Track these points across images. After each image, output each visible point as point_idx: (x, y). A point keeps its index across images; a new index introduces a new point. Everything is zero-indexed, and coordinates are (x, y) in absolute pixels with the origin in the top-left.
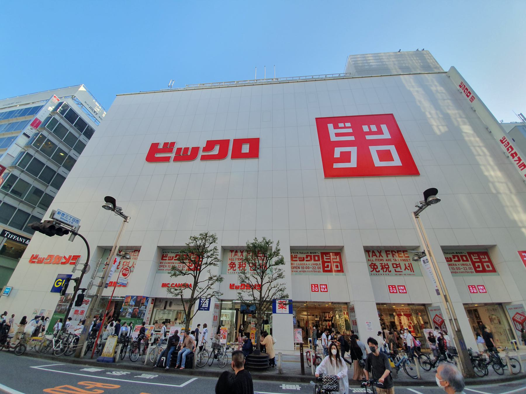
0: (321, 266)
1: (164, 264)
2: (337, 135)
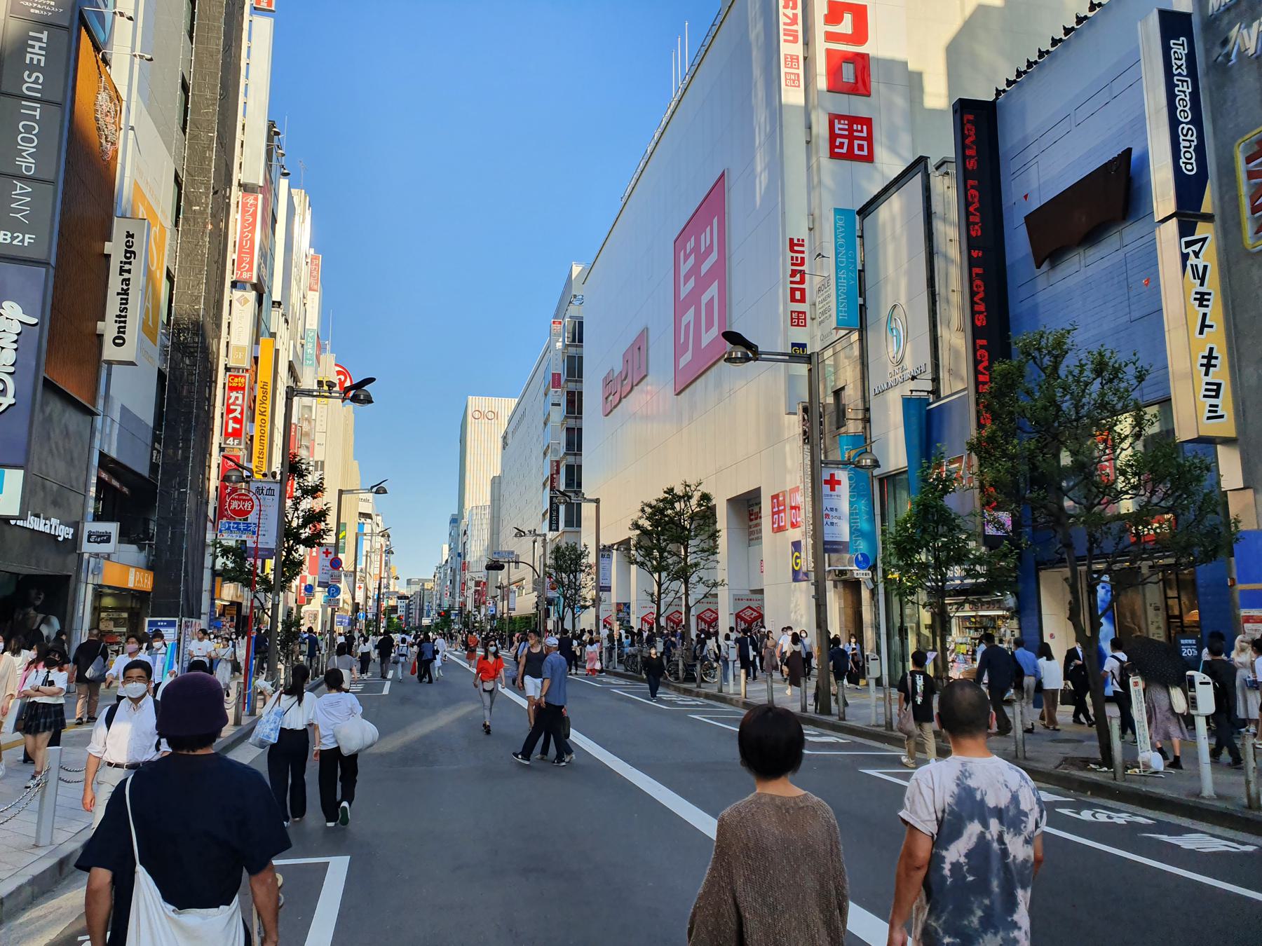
2: (840, 129)
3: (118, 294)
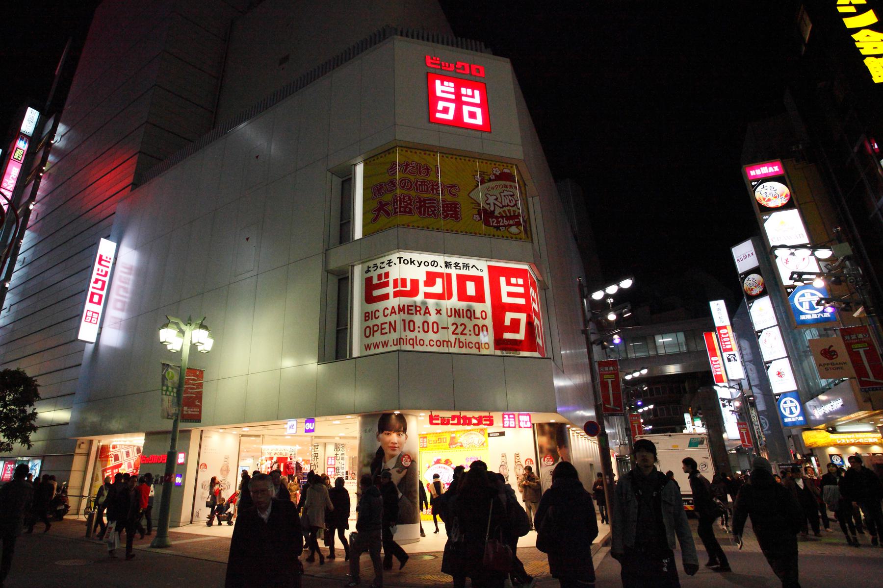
0: (489, 322)
1: (382, 319)
2: (510, 294)
3: (411, 259)
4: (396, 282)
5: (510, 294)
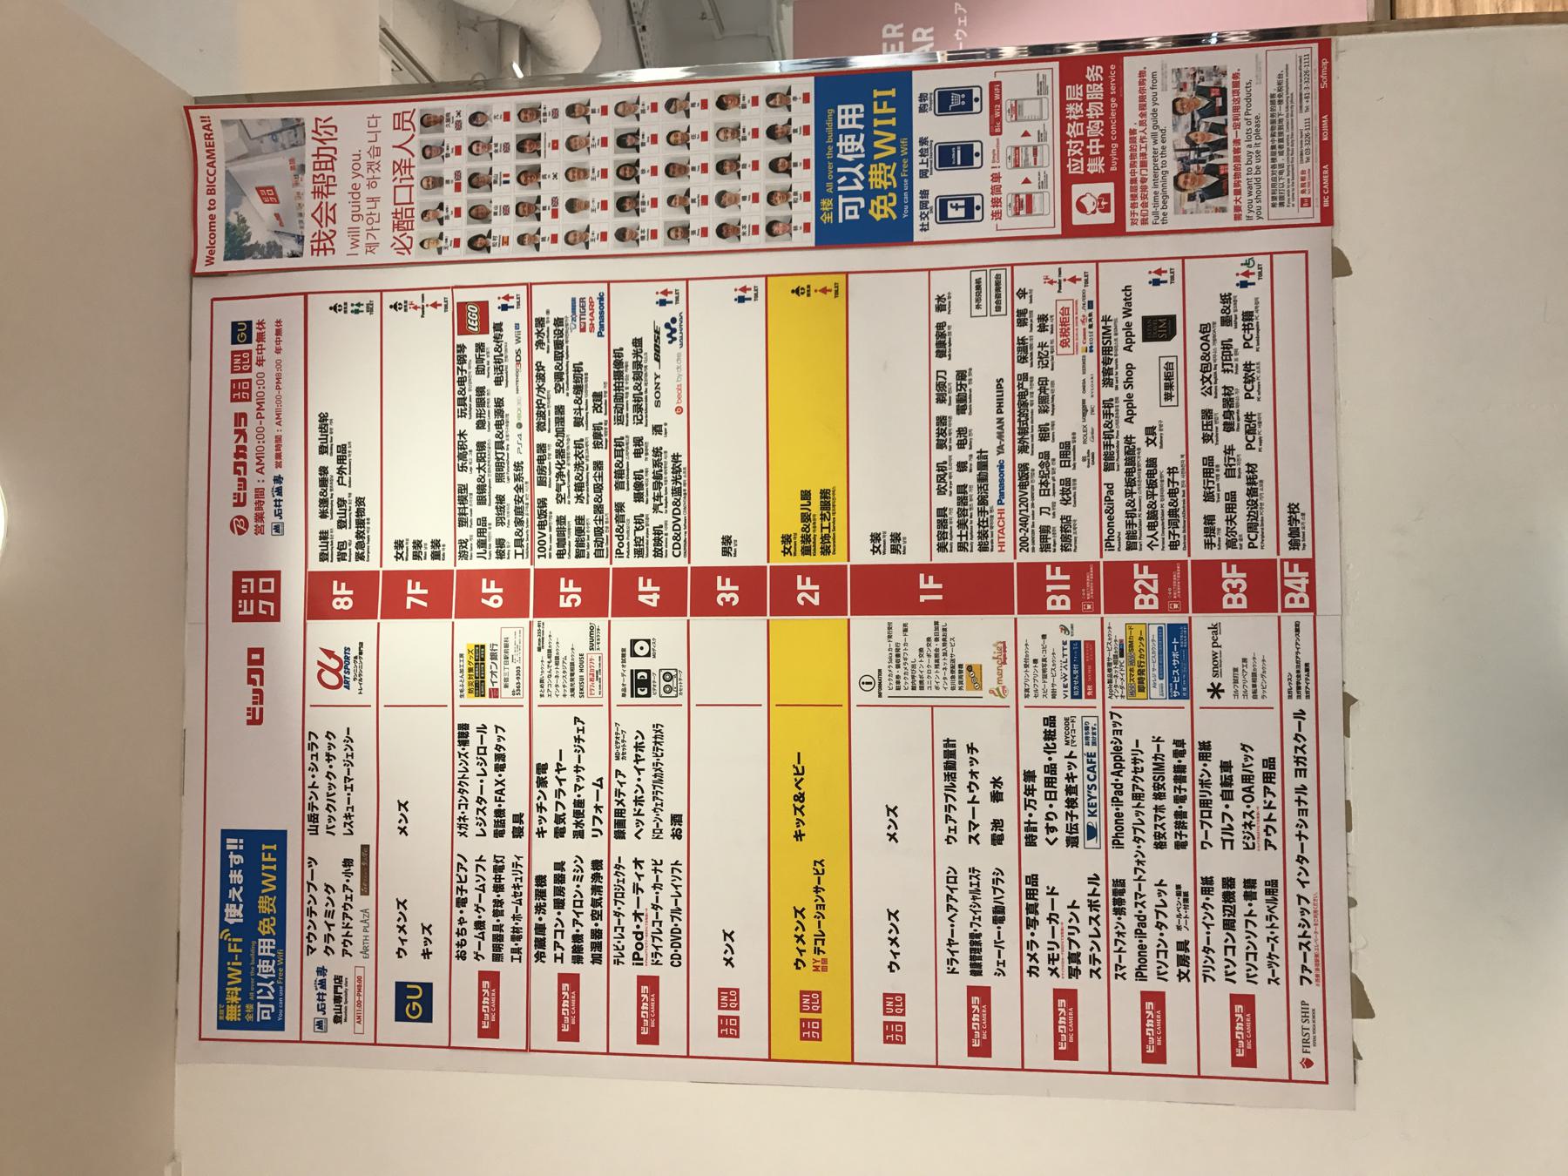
2: (249, 609)
4: (254, 703)
5: (249, 609)
